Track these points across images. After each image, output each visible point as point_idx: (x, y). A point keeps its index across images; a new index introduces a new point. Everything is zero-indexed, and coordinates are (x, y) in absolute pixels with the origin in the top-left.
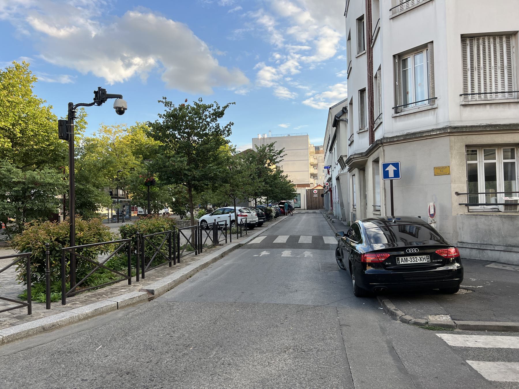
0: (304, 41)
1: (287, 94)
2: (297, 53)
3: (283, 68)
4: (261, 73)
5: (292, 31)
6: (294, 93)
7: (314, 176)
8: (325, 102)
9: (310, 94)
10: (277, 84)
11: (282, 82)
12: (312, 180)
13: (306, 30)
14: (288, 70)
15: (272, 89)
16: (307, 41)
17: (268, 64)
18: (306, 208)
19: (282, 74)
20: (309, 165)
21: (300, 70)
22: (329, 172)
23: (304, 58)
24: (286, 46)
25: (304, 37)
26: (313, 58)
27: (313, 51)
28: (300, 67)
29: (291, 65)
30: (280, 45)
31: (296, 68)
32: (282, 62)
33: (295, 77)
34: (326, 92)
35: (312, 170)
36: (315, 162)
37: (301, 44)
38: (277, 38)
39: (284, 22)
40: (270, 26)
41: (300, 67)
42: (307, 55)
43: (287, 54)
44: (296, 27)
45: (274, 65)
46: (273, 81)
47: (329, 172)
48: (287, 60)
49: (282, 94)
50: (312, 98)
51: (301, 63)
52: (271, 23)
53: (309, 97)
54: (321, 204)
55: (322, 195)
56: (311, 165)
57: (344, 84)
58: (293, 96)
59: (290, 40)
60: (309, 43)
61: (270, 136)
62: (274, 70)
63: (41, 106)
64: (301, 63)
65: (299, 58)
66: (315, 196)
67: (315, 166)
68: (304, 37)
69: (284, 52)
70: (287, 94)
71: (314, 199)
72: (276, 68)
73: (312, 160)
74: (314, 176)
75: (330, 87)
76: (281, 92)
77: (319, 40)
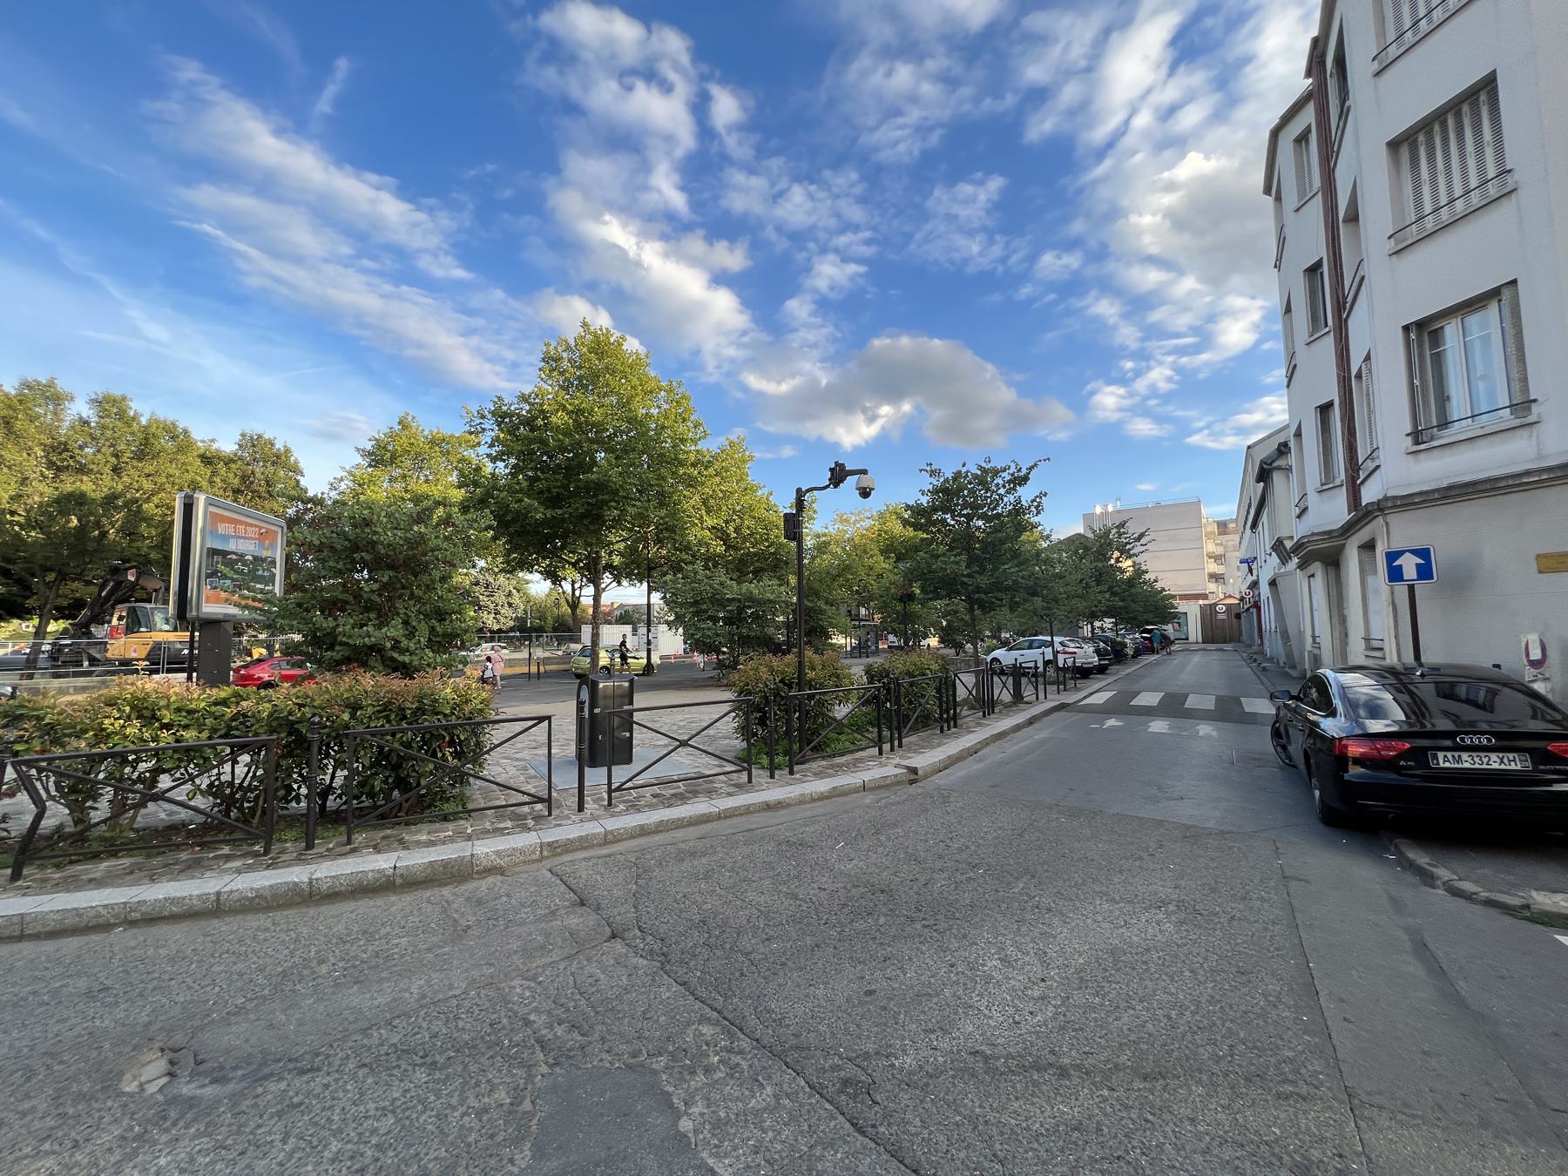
0: (1184, 329)
2: (1169, 353)
3: (1141, 385)
4: (1098, 398)
7: (1216, 577)
9: (1201, 424)
11: (1140, 409)
15: (1119, 424)
22: (1251, 571)
23: (1184, 360)
24: (1147, 344)
26: (1204, 357)
29: (1159, 376)
32: (1138, 373)
35: (1213, 567)
36: (1220, 550)
37: (1178, 335)
38: (1128, 335)
45: (1123, 381)
47: (1251, 571)
48: (1149, 368)
55: (1238, 616)
59: (1155, 332)
60: (1194, 330)
66: (1221, 617)
67: (1217, 558)
68: (1183, 321)
73: (1210, 547)
74: (1216, 577)
75: (1246, 406)
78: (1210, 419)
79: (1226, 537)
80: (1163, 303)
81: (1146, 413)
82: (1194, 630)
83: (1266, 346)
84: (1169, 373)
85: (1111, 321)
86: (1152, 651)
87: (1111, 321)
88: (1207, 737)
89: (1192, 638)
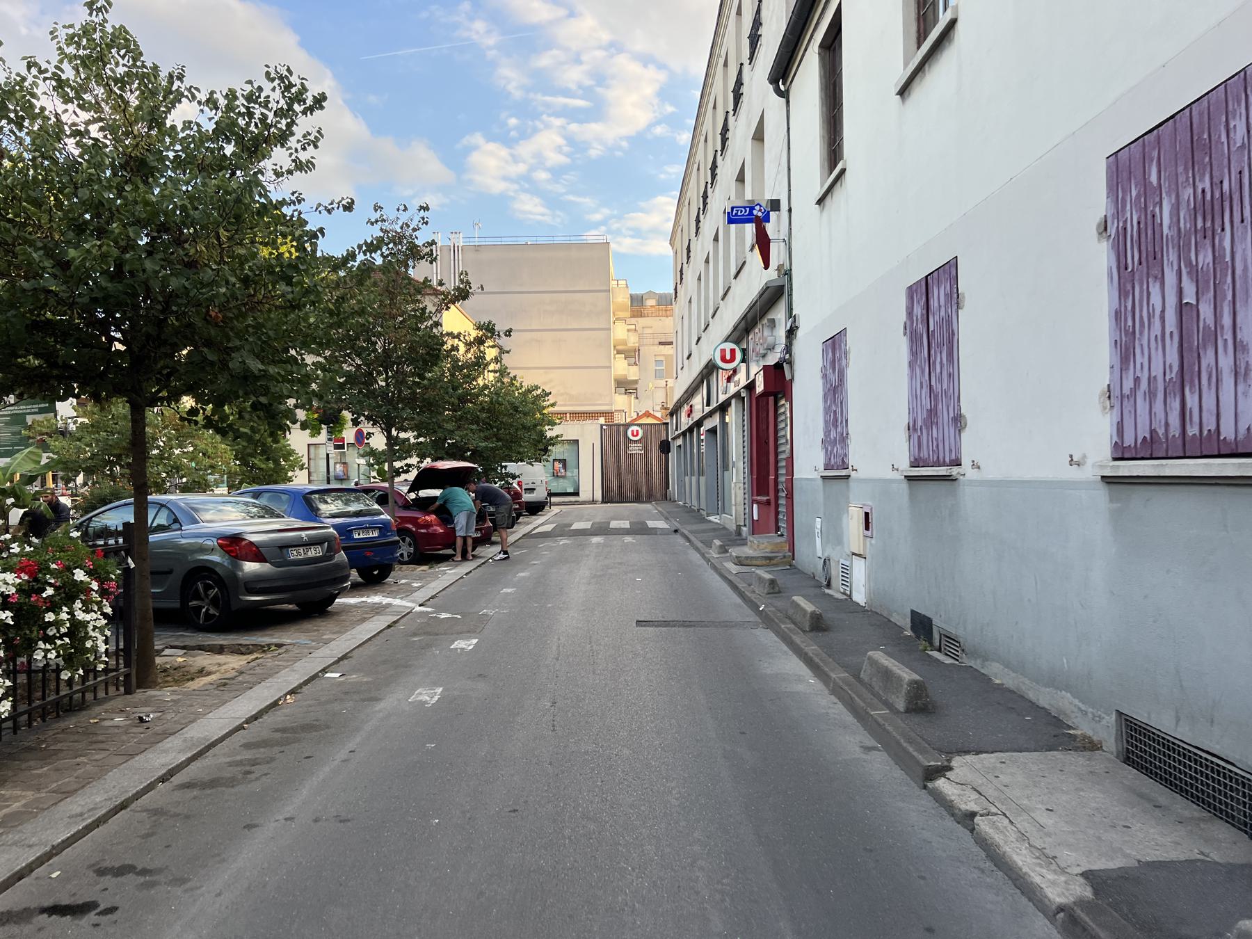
0: (573, 87)
1: (543, 215)
2: (557, 115)
3: (525, 149)
4: (475, 158)
5: (544, 61)
6: (558, 213)
7: (626, 386)
8: (632, 237)
9: (597, 217)
10: (516, 187)
11: (527, 183)
12: (620, 401)
13: (577, 60)
14: (539, 156)
15: (503, 199)
16: (580, 86)
17: (490, 138)
18: (598, 496)
19: (524, 162)
20: (613, 352)
21: (567, 155)
22: (763, 243)
23: (574, 127)
24: (532, 95)
25: (574, 76)
26: (595, 128)
27: (597, 112)
28: (566, 149)
29: (548, 142)
30: (518, 94)
31: (559, 149)
32: (525, 134)
33: (557, 172)
34: (632, 214)
35: (621, 367)
36: (633, 341)
37: (566, 93)
38: (510, 77)
39: (526, 40)
40: (490, 48)
41: (566, 149)
42: (580, 122)
43: (536, 116)
44: (555, 52)
45: (508, 142)
46: (506, 178)
47: (763, 243)
48: (535, 131)
49: (530, 213)
50: (603, 228)
51: (570, 140)
52: (491, 41)
53: (596, 225)
54: (658, 478)
55: (665, 447)
56: (619, 352)
57: (673, 197)
58: (558, 220)
59: (543, 82)
60: (587, 93)
61: (476, 242)
62: (504, 152)
63: (768, 576)
64: (570, 140)
65: (563, 127)
66: (634, 449)
67: (632, 355)
68: (574, 76)
69: (527, 112)
70: (543, 215)
71: (631, 461)
72: (510, 147)
73: (620, 332)
74: (626, 386)
75: (642, 204)
76: (527, 207)
77: (608, 87)
78: (606, 211)
79: (642, 322)
80: (549, 46)
81: (533, 188)
82: (589, 479)
83: (659, 130)
84: (560, 141)
85: (492, 54)
86: (431, 551)
87: (492, 54)
88: (598, 545)
89: (585, 494)
